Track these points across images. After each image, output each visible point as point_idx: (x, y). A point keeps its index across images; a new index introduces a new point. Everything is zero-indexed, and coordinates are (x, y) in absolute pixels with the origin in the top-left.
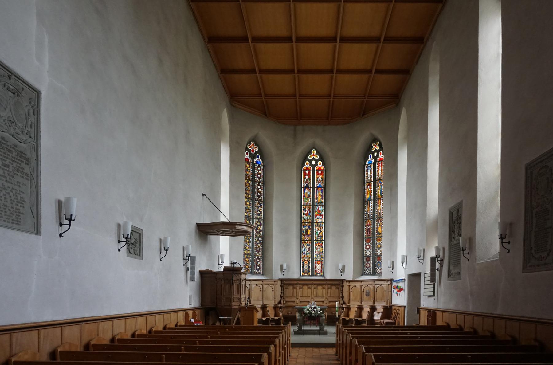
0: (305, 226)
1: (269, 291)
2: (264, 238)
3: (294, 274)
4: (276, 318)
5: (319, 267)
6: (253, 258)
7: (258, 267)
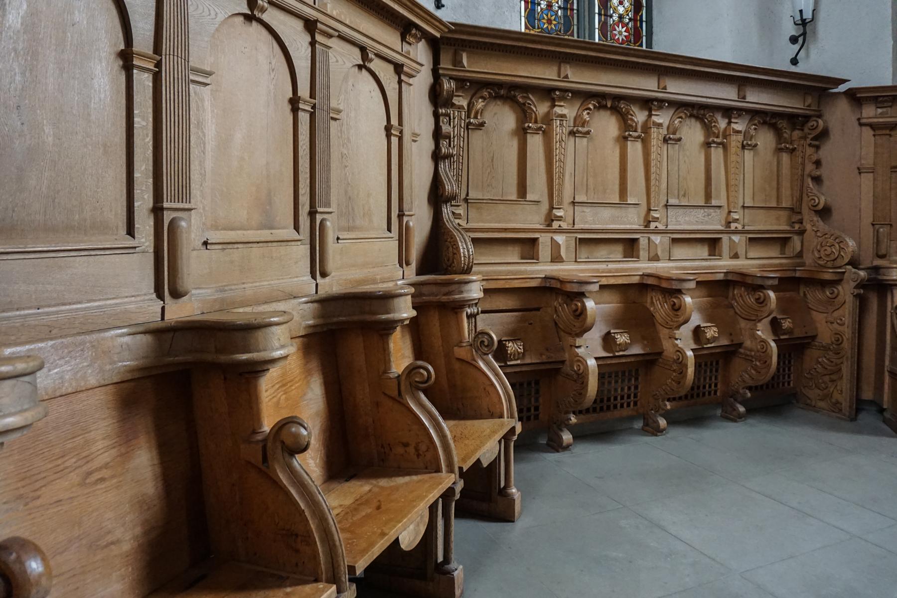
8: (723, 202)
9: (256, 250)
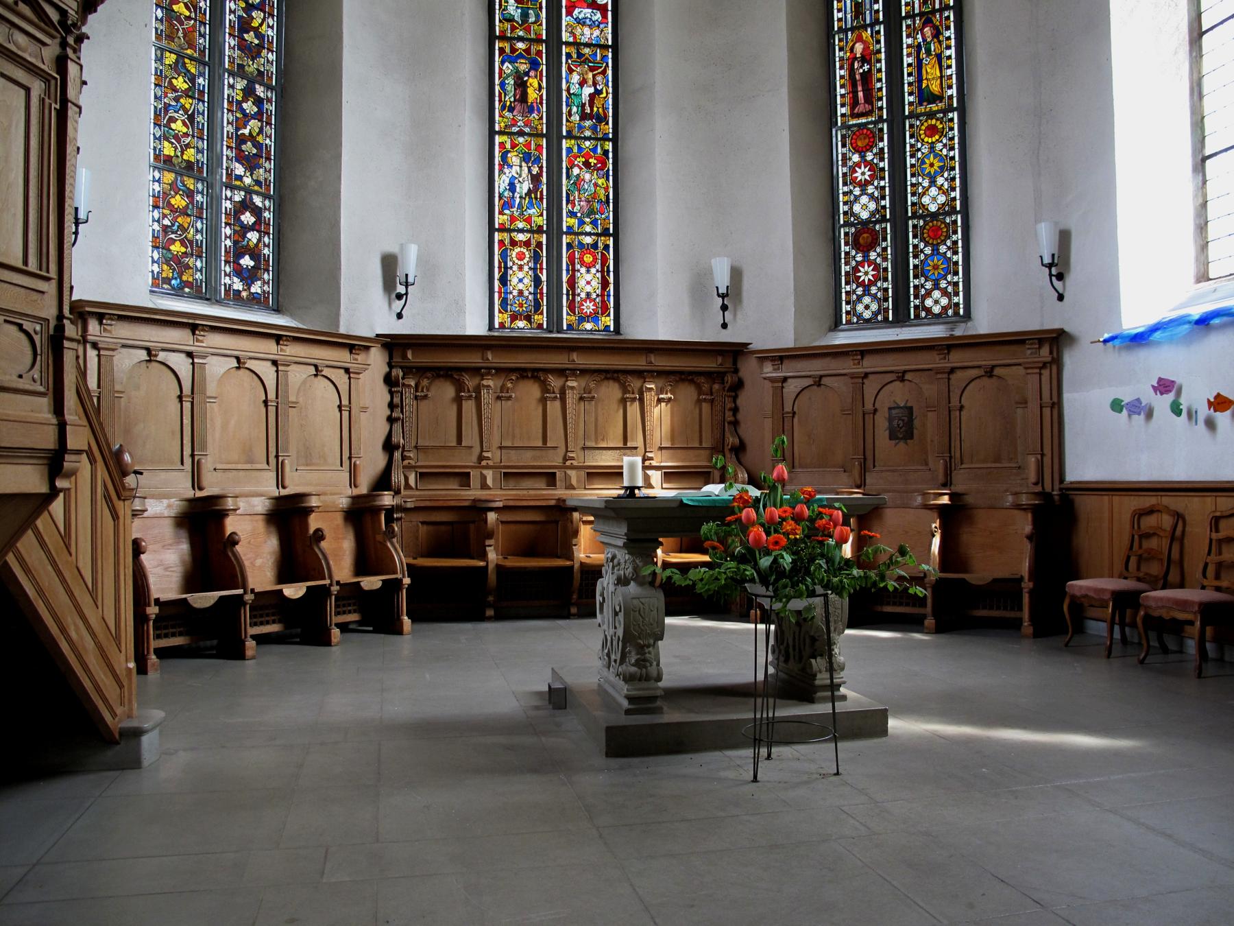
0: (512, 57)
1: (317, 401)
2: (283, 91)
3: (462, 307)
4: (372, 583)
5: (588, 282)
6: (214, 201)
7: (247, 261)
8: (639, 442)
9: (241, 473)
